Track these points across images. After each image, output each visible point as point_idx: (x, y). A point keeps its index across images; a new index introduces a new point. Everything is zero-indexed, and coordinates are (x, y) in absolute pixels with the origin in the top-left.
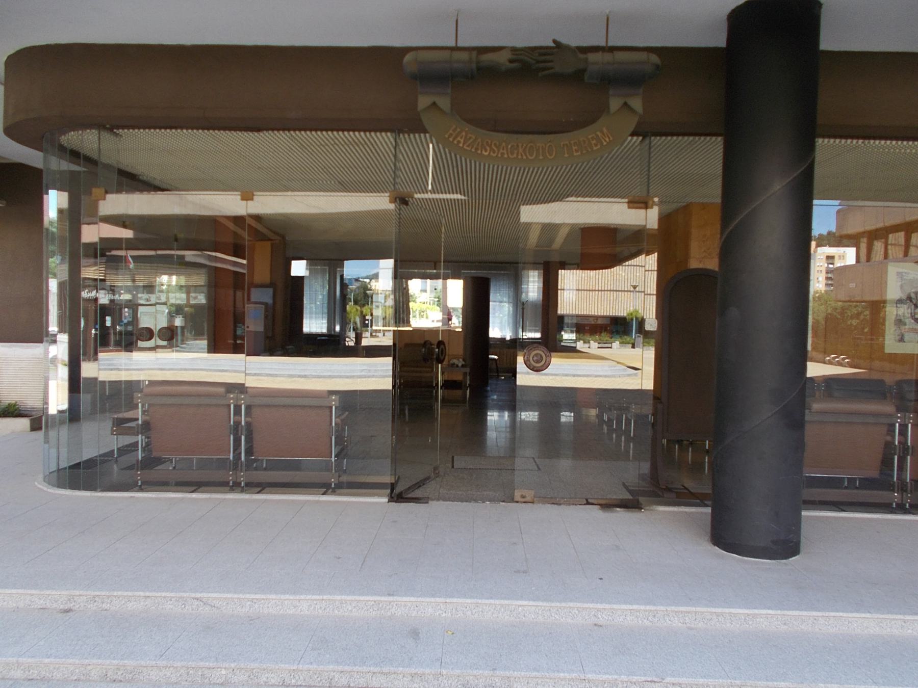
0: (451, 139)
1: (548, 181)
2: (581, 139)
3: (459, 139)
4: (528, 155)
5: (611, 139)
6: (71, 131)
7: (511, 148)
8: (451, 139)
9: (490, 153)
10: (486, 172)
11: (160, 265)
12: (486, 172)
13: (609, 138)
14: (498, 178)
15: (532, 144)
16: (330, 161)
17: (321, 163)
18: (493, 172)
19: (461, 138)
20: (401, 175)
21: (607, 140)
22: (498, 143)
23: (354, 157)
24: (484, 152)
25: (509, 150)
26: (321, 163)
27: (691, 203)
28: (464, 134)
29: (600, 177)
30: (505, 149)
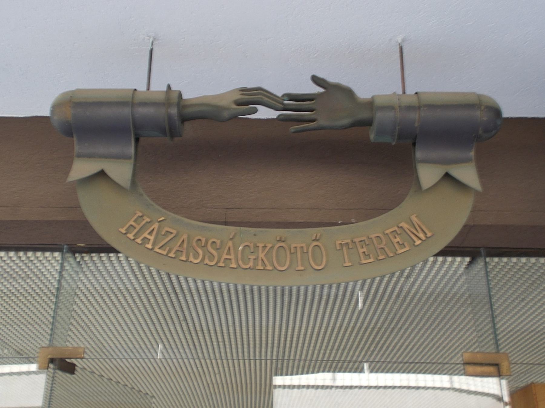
0: (131, 236)
1: (463, 338)
2: (373, 236)
3: (146, 235)
4: (275, 263)
5: (429, 235)
6: (276, 118)
7: (243, 249)
8: (131, 236)
9: (203, 260)
10: (311, 348)
11: (126, 111)
12: (311, 348)
13: (425, 234)
14: (258, 382)
15: (316, 243)
16: (110, 342)
17: (213, 400)
18: (456, 312)
19: (150, 233)
20: (526, 380)
21: (422, 235)
22: (218, 242)
23: (105, 308)
24: (191, 259)
25: (240, 256)
26: (213, 400)
27: (532, 383)
28: (156, 226)
29: (308, 323)
30: (232, 251)
